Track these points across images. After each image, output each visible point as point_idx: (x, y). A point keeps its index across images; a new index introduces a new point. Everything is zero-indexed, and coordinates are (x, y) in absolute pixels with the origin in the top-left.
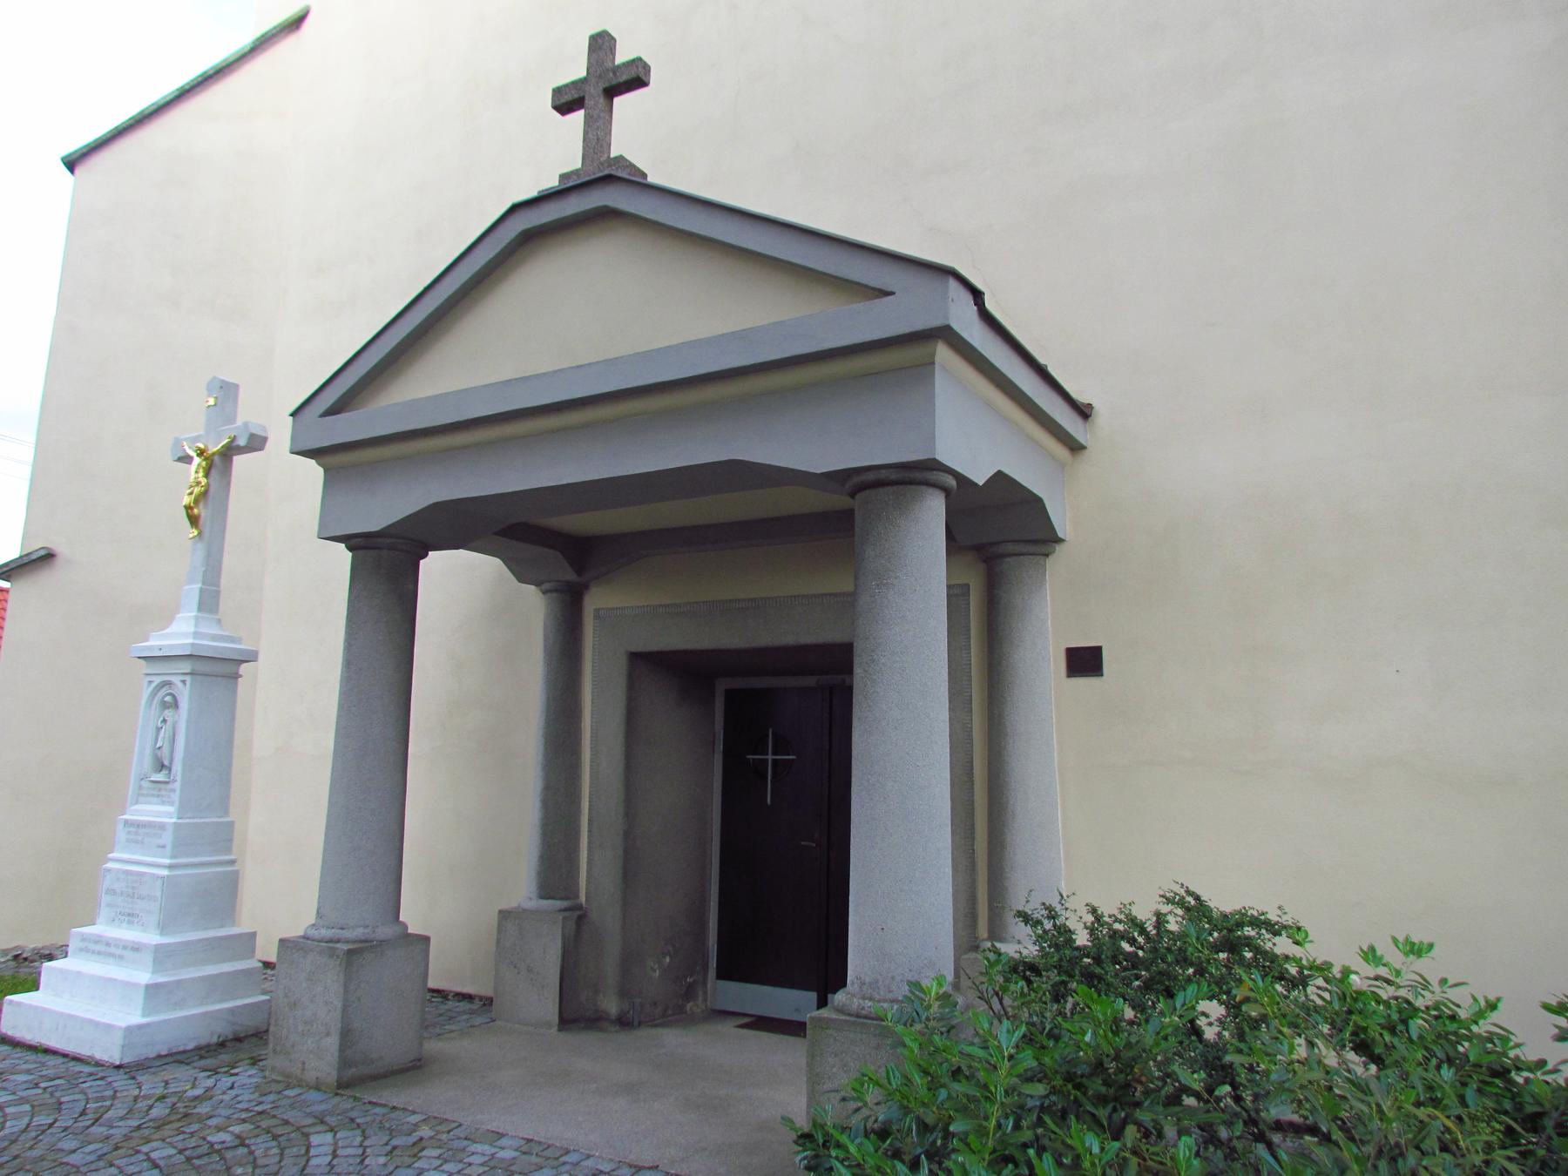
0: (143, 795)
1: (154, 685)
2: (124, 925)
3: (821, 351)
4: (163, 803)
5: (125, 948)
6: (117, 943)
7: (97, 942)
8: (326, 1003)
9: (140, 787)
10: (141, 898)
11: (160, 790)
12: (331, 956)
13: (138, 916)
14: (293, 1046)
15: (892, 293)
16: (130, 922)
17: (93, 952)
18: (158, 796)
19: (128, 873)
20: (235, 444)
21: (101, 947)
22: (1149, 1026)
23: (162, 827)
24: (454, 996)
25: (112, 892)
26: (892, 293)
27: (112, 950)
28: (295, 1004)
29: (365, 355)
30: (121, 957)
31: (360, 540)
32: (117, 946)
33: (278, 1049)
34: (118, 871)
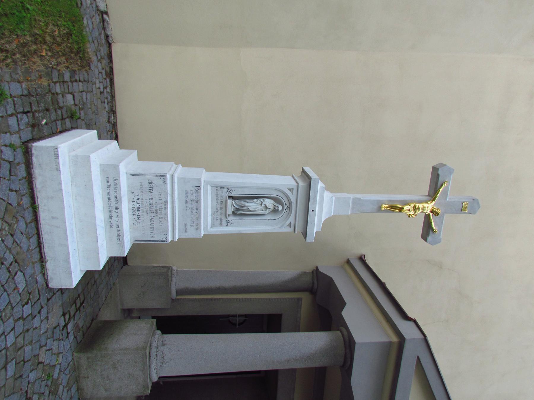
0: (217, 191)
1: (289, 193)
2: (131, 206)
3: (400, 370)
4: (213, 214)
5: (118, 227)
6: (119, 219)
7: (116, 195)
8: (121, 387)
9: (222, 188)
10: (152, 218)
11: (221, 208)
12: (144, 386)
13: (139, 219)
14: (94, 370)
15: (418, 358)
16: (134, 209)
17: (109, 194)
18: (217, 208)
19: (166, 203)
20: (431, 232)
21: (113, 204)
22: (162, 347)
23: (198, 228)
24: (111, 67)
25: (158, 334)
26: (418, 358)
27: (114, 214)
28: (115, 368)
29: (437, 377)
30: (111, 225)
31: (349, 363)
32: (117, 220)
33: (90, 360)
34: (166, 192)
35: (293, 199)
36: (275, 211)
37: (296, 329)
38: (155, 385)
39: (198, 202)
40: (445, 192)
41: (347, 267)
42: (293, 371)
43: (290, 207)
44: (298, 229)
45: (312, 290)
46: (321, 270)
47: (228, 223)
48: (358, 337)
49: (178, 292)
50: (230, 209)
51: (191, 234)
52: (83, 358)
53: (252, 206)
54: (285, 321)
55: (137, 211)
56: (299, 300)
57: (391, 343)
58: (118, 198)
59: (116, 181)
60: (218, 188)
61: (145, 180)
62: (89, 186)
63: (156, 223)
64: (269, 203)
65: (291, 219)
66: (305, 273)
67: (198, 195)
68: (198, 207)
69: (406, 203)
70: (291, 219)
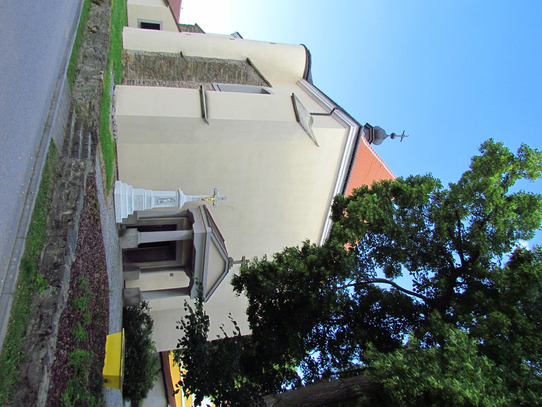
6: (132, 206)
35: (175, 199)
36: (171, 201)
37: (182, 229)
38: (139, 245)
39: (151, 201)
40: (217, 195)
41: (199, 209)
42: (181, 241)
43: (175, 201)
44: (177, 206)
45: (187, 217)
46: (190, 210)
47: (159, 205)
48: (195, 232)
49: (140, 218)
50: (159, 202)
51: (149, 208)
52: (121, 238)
53: (165, 201)
54: (178, 227)
55: (135, 204)
56: (183, 220)
57: (204, 233)
58: (131, 202)
59: (131, 198)
60: (156, 197)
61: (138, 197)
62: (125, 200)
63: (140, 206)
64: (169, 200)
65: (175, 204)
66: (184, 211)
67: (151, 199)
68: (151, 202)
69: (206, 198)
70: (175, 204)
